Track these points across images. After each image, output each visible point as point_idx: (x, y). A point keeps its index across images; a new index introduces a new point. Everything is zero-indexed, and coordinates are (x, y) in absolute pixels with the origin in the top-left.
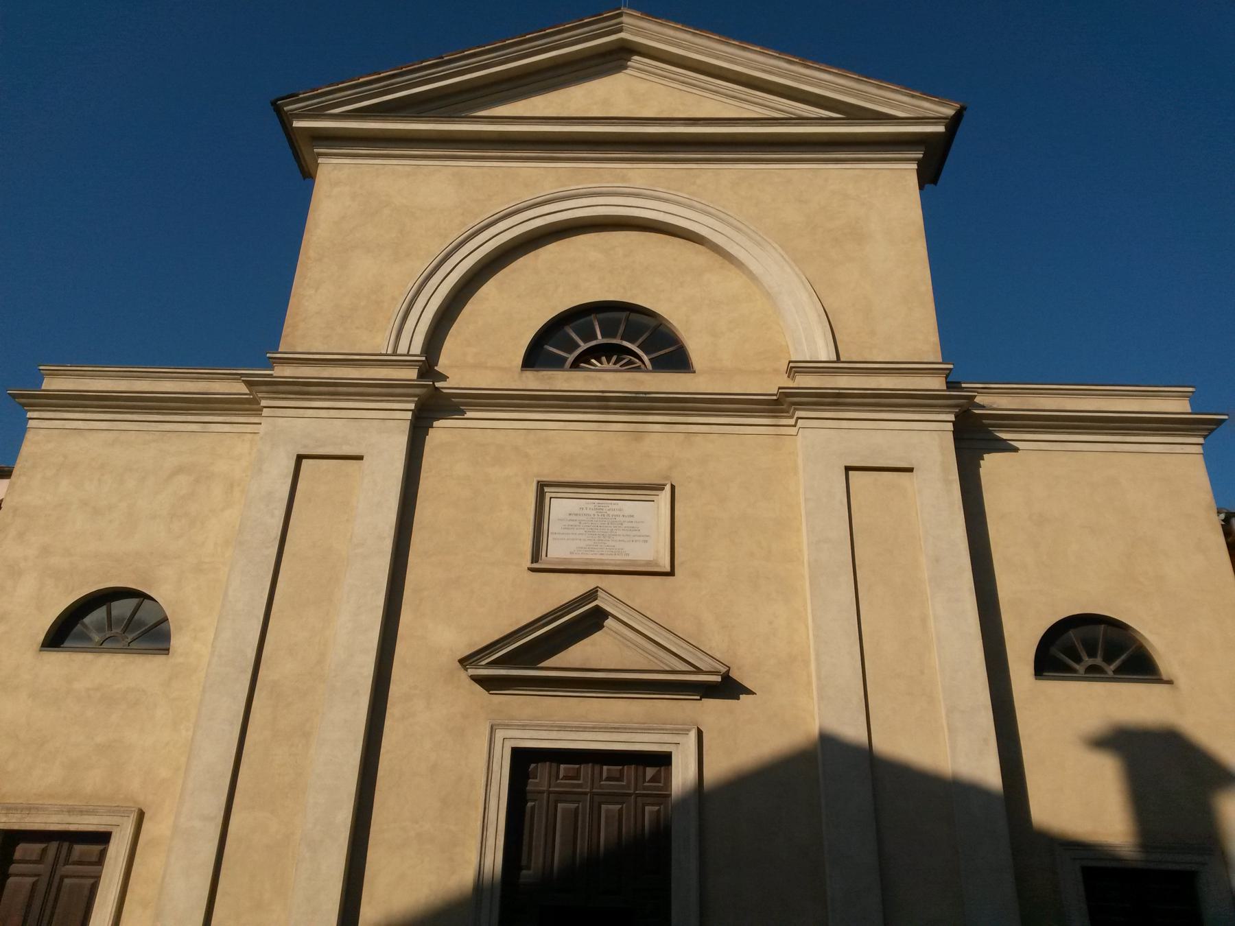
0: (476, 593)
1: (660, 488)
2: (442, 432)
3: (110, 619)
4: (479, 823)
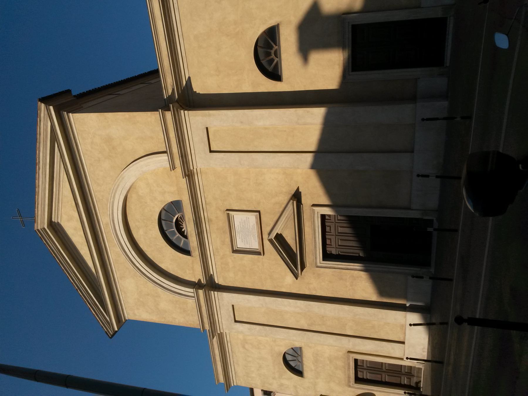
0: (273, 271)
1: (228, 214)
2: (219, 280)
3: (293, 363)
4: (347, 271)
